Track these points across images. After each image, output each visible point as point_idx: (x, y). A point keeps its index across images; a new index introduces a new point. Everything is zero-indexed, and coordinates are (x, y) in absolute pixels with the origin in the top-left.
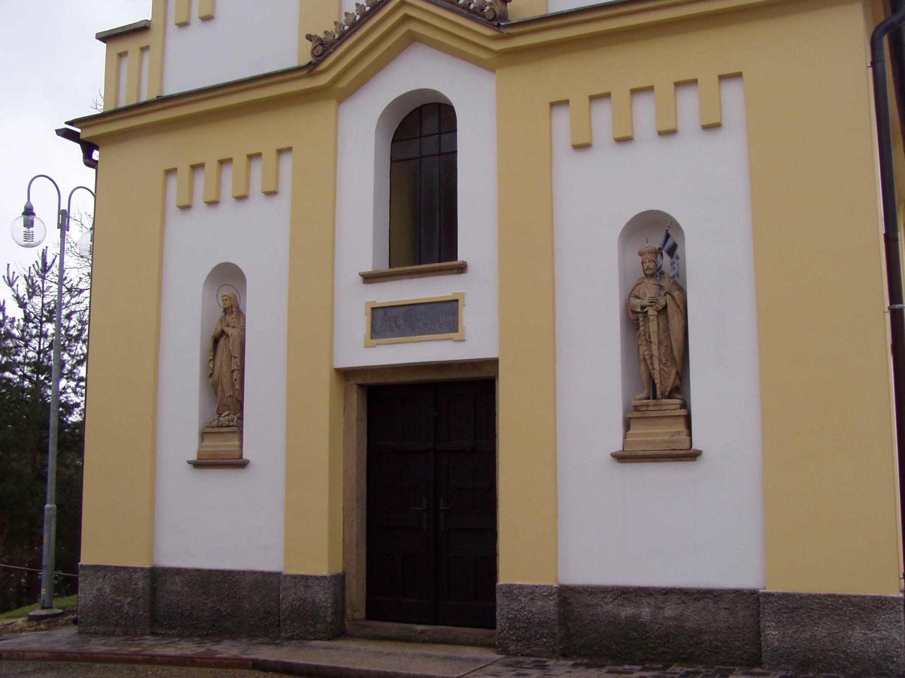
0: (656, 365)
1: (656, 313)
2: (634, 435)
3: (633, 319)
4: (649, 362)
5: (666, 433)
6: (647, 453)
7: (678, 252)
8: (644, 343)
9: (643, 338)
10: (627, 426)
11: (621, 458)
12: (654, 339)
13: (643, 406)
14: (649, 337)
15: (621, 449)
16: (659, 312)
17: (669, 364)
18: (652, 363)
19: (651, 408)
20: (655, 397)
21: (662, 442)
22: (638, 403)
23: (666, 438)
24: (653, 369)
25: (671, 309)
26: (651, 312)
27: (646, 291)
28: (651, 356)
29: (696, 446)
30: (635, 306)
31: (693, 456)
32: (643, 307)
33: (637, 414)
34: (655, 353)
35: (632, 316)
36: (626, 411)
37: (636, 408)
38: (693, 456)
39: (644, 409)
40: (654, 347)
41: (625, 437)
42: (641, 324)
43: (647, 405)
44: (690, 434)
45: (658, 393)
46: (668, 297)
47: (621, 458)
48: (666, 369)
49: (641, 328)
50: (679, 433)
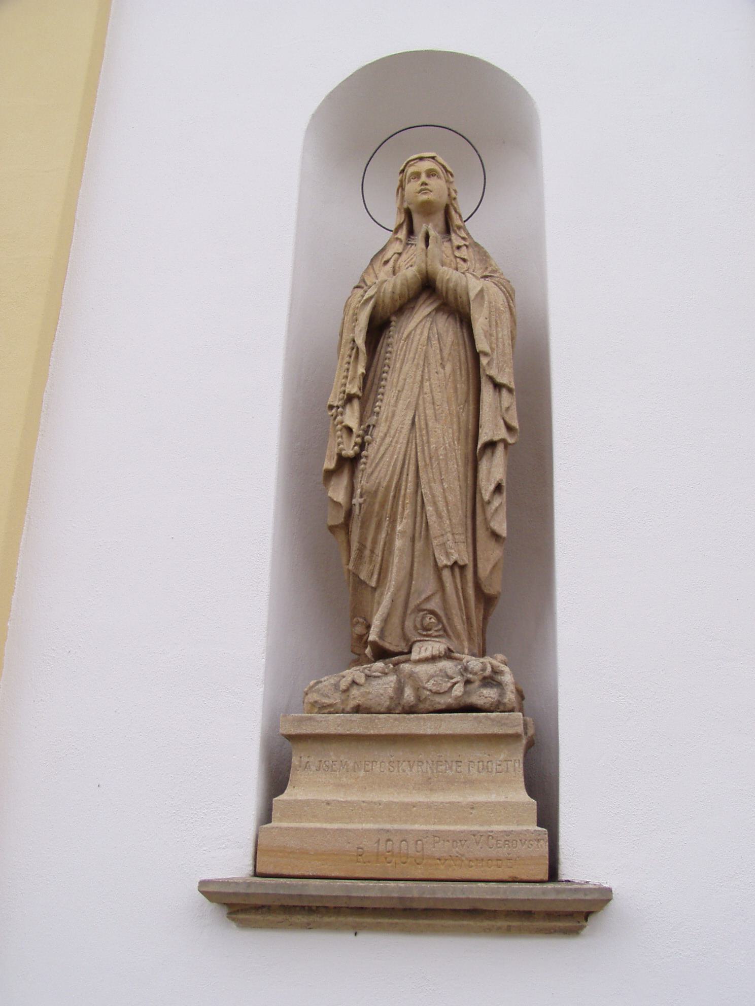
44: (548, 818)
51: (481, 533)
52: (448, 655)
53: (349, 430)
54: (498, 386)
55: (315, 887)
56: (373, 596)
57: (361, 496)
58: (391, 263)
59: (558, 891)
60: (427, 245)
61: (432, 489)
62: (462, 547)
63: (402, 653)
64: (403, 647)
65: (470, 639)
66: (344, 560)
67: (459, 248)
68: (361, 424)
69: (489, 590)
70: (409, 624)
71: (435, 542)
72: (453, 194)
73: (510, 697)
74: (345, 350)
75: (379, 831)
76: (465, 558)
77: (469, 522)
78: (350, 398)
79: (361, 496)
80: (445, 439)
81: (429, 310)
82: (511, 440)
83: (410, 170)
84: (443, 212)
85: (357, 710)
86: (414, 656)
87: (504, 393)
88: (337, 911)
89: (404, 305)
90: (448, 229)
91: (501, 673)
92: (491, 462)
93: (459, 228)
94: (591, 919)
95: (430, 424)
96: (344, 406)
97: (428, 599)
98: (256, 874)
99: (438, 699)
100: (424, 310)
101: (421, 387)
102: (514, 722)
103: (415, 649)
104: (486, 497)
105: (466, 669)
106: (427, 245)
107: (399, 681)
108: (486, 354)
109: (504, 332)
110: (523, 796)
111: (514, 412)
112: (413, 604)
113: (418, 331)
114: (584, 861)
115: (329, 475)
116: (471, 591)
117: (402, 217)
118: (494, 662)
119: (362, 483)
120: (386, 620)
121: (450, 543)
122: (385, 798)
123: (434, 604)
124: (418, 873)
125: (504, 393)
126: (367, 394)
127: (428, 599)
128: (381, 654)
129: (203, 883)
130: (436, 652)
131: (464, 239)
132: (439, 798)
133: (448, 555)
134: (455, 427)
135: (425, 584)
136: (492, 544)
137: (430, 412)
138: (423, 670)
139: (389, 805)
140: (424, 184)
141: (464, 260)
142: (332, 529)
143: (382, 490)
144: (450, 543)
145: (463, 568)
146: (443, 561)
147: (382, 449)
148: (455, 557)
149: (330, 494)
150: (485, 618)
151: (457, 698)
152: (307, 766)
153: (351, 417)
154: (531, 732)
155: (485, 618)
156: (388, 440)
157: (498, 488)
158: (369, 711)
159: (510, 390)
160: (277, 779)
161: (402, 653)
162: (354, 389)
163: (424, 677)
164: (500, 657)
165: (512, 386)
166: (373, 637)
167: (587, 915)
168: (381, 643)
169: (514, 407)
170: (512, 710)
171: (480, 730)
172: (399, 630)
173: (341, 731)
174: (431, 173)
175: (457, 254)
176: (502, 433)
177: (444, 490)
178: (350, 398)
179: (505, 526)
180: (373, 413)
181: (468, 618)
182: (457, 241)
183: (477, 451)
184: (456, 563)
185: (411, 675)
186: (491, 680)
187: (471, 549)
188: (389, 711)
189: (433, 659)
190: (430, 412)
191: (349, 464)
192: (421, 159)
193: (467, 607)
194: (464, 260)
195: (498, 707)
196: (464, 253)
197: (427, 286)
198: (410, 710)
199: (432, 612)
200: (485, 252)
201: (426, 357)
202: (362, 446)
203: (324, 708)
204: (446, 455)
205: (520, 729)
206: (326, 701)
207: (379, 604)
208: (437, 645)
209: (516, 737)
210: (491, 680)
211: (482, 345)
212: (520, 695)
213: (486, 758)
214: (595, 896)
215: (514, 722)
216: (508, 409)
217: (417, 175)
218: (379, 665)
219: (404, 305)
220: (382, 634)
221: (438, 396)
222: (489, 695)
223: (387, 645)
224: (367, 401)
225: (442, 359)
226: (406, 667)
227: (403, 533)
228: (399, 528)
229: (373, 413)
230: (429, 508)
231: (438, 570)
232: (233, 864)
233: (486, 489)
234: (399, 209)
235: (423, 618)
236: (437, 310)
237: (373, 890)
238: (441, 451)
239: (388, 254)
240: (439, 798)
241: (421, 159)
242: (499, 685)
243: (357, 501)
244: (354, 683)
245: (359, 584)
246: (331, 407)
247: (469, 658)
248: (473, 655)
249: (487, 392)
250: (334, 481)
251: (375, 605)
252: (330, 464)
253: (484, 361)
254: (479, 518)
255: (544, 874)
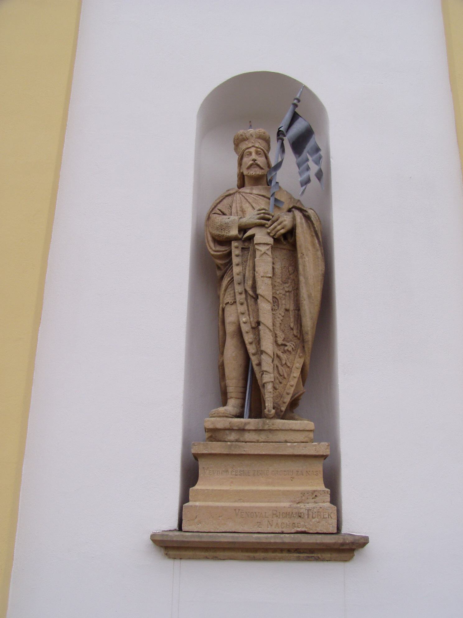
0: (268, 345)
1: (271, 241)
2: (207, 495)
3: (218, 258)
4: (248, 338)
5: (286, 494)
6: (242, 538)
7: (316, 139)
8: (240, 298)
9: (238, 289)
10: (190, 476)
11: (173, 546)
12: (264, 289)
13: (231, 430)
14: (254, 287)
15: (174, 525)
16: (277, 240)
17: (290, 346)
18: (258, 341)
19: (248, 436)
20: (257, 411)
21: (276, 513)
22: (221, 423)
23: (285, 504)
24: (260, 352)
25: (303, 236)
26: (261, 237)
27: (246, 206)
28: (257, 326)
29: (352, 526)
30: (227, 227)
31: (346, 549)
32: (243, 229)
33: (216, 448)
34: (266, 318)
35: (213, 249)
36: (187, 444)
37: (214, 434)
38: (346, 549)
39: (233, 436)
40: (265, 307)
41: (185, 498)
42: (235, 260)
43: (242, 430)
44: (335, 499)
45: (269, 404)
46: (298, 215)
47: (173, 546)
48: (284, 357)
49: (236, 270)
50: (314, 494)
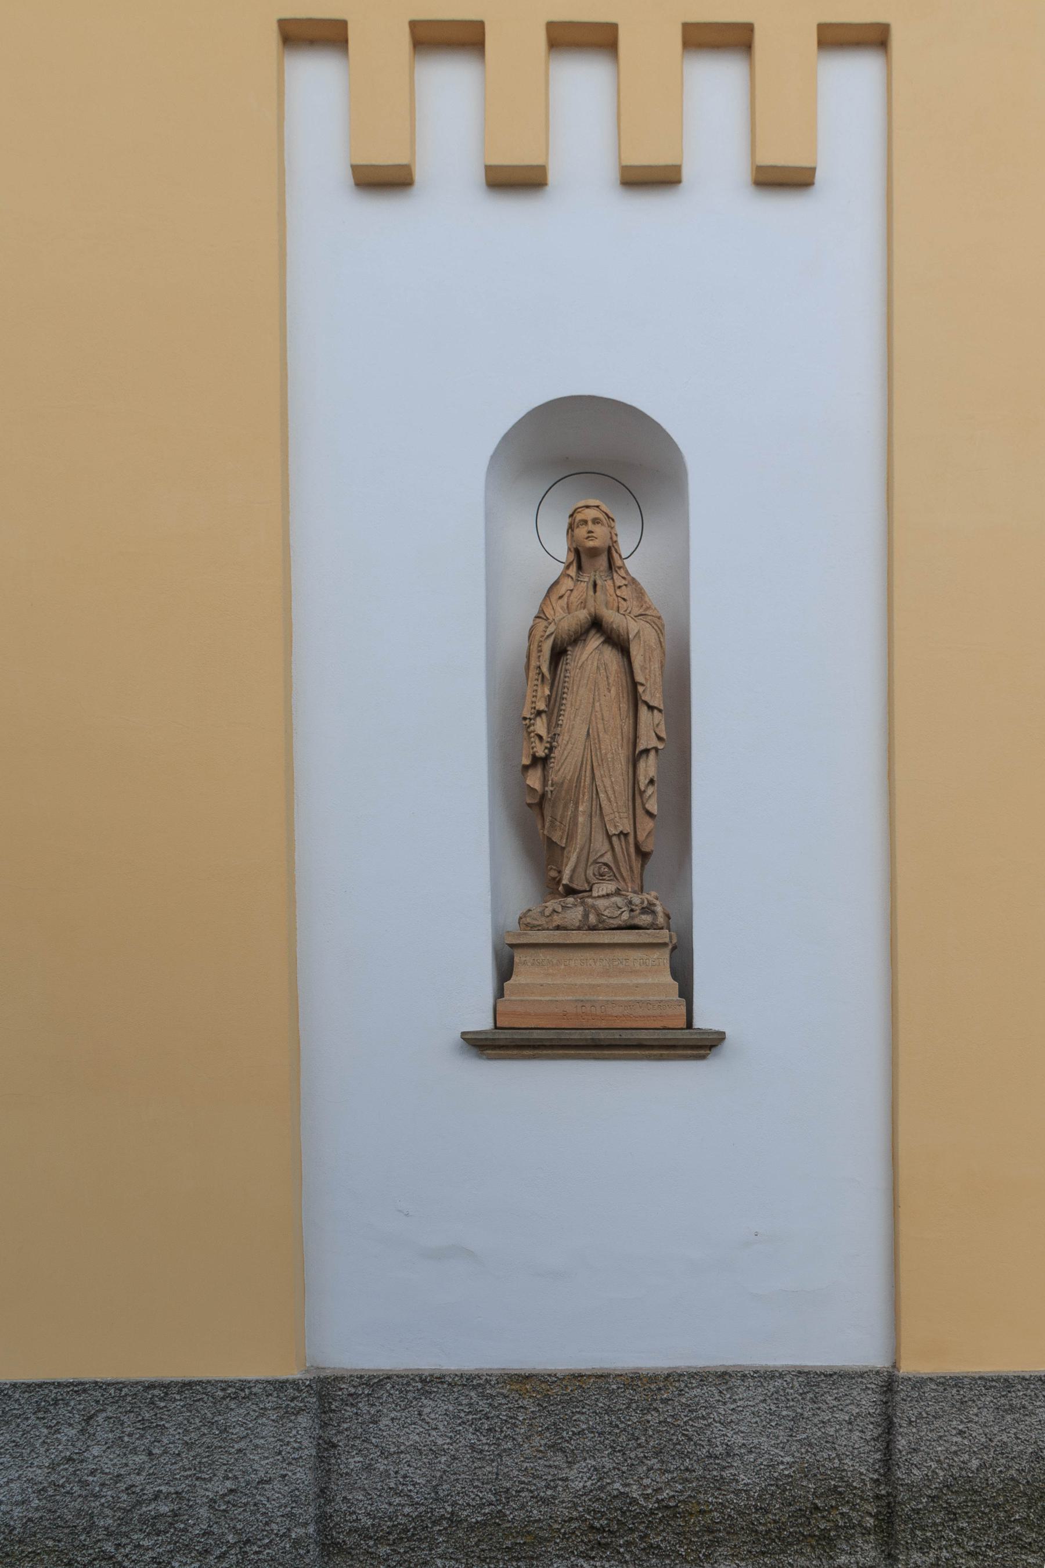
11: (482, 1045)
31: (704, 1046)
38: (704, 1046)
44: (686, 992)
51: (640, 812)
52: (618, 892)
53: (540, 738)
54: (651, 708)
55: (536, 1035)
56: (562, 854)
57: (552, 785)
58: (565, 599)
59: (691, 1034)
60: (595, 591)
61: (604, 782)
62: (625, 821)
63: (586, 891)
64: (586, 887)
65: (633, 881)
66: (539, 827)
67: (620, 587)
68: (548, 733)
69: (646, 849)
70: (590, 872)
71: (606, 819)
72: (615, 538)
73: (661, 920)
74: (533, 673)
75: (576, 1001)
76: (628, 828)
77: (630, 804)
78: (539, 713)
79: (552, 785)
80: (614, 748)
81: (598, 642)
82: (660, 746)
83: (579, 517)
84: (606, 553)
85: (558, 928)
86: (595, 894)
87: (655, 711)
88: (552, 1047)
89: (578, 638)
90: (611, 566)
91: (654, 905)
92: (646, 762)
93: (620, 568)
94: (713, 1050)
95: (601, 735)
96: (534, 719)
97: (602, 856)
98: (496, 1028)
99: (611, 921)
100: (594, 642)
101: (593, 706)
102: (663, 936)
103: (595, 887)
104: (643, 788)
105: (630, 902)
106: (595, 591)
107: (585, 910)
108: (642, 685)
109: (656, 666)
110: (668, 979)
111: (662, 726)
112: (591, 861)
113: (590, 662)
114: (707, 1017)
115: (526, 768)
116: (632, 850)
117: (572, 556)
118: (648, 897)
119: (553, 777)
120: (574, 871)
121: (617, 819)
122: (579, 981)
123: (608, 858)
124: (603, 1025)
125: (655, 711)
126: (553, 710)
127: (602, 856)
128: (570, 891)
129: (463, 1033)
130: (609, 892)
131: (624, 578)
132: (613, 981)
133: (616, 827)
134: (619, 737)
135: (600, 845)
136: (647, 819)
137: (600, 726)
138: (601, 903)
139: (581, 986)
140: (590, 532)
141: (624, 600)
142: (530, 805)
143: (565, 786)
144: (617, 819)
145: (626, 835)
146: (612, 831)
147: (566, 753)
148: (621, 828)
149: (528, 782)
150: (643, 866)
151: (625, 921)
152: (525, 963)
153: (540, 726)
154: (675, 941)
155: (643, 866)
156: (570, 746)
157: (652, 782)
158: (565, 929)
159: (660, 711)
160: (504, 971)
161: (586, 891)
162: (541, 706)
163: (602, 908)
164: (653, 893)
165: (662, 707)
166: (565, 881)
167: (711, 1047)
168: (571, 885)
169: (663, 722)
170: (662, 928)
171: (641, 940)
172: (583, 876)
173: (547, 941)
174: (596, 521)
175: (618, 593)
176: (654, 743)
177: (613, 780)
178: (539, 713)
179: (656, 807)
180: (557, 725)
181: (631, 867)
182: (619, 582)
183: (636, 756)
184: (621, 832)
185: (593, 907)
186: (648, 909)
187: (632, 822)
188: (579, 929)
189: (608, 896)
190: (600, 726)
191: (541, 762)
192: (587, 507)
193: (629, 855)
194: (624, 600)
195: (653, 926)
196: (624, 592)
197: (596, 624)
198: (593, 928)
199: (606, 864)
200: (641, 589)
201: (596, 683)
202: (551, 749)
203: (533, 927)
204: (613, 758)
205: (667, 940)
206: (536, 923)
207: (569, 858)
208: (610, 886)
209: (665, 945)
210: (648, 909)
211: (639, 678)
212: (668, 917)
213: (645, 957)
214: (715, 1036)
215: (663, 936)
216: (658, 725)
217: (585, 522)
218: (570, 900)
219: (578, 638)
220: (571, 879)
221: (606, 714)
222: (646, 919)
223: (575, 886)
224: (552, 713)
225: (609, 684)
226: (590, 901)
227: (584, 812)
228: (581, 809)
229: (557, 725)
230: (602, 795)
231: (609, 837)
232: (482, 1022)
233: (643, 781)
234: (569, 549)
235: (600, 868)
236: (604, 642)
237: (576, 1035)
238: (609, 756)
239: (563, 589)
240: (613, 981)
241: (587, 507)
242: (654, 912)
243: (549, 788)
244: (554, 911)
245: (551, 843)
246: (525, 719)
247: (632, 895)
248: (635, 892)
249: (643, 711)
250: (531, 772)
251: (565, 860)
252: (526, 761)
253: (640, 689)
254: (638, 801)
255: (682, 1023)
